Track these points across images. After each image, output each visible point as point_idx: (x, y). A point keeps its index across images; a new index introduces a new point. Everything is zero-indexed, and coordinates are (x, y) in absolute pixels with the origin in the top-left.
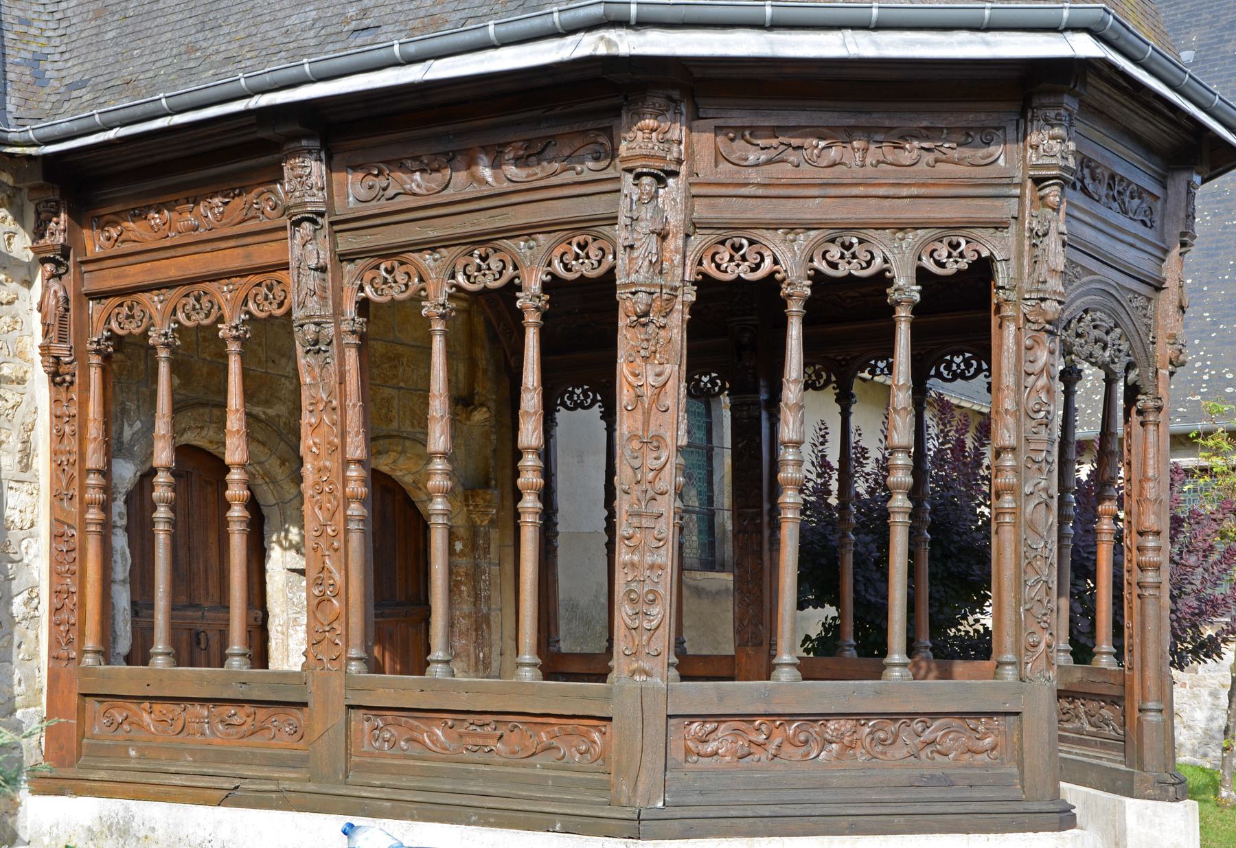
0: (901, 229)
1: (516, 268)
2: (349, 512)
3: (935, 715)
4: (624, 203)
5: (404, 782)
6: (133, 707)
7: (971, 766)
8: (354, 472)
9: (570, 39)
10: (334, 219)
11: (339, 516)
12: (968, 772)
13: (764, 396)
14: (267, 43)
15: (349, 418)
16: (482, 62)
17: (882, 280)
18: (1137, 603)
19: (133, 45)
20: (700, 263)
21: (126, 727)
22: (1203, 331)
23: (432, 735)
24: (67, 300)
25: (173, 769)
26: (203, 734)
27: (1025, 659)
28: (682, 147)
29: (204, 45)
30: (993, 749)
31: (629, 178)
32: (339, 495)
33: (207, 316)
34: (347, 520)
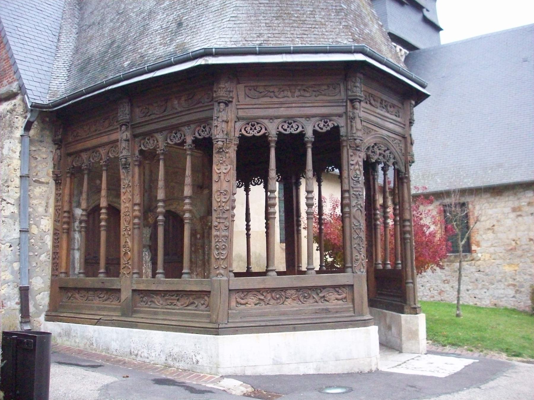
7: (337, 305)
13: (294, 181)
17: (302, 135)
21: (72, 298)
24: (61, 156)
27: (354, 265)
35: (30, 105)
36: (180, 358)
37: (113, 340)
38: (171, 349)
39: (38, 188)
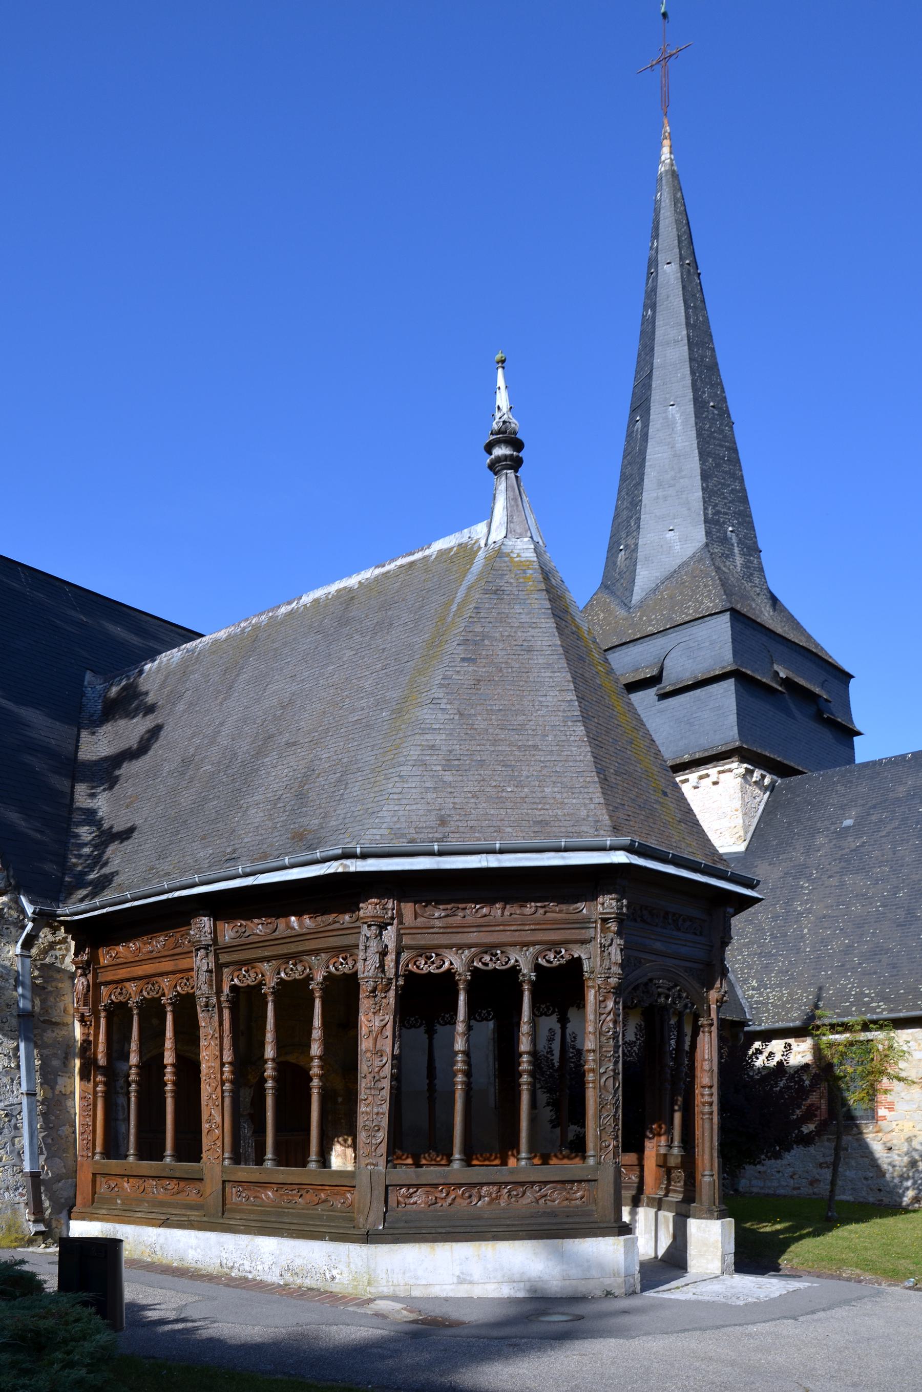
0: (525, 946)
1: (310, 970)
2: (224, 1088)
3: (546, 1183)
4: (362, 939)
5: (252, 1217)
6: (120, 1180)
8: (227, 1068)
9: (328, 864)
10: (216, 947)
11: (219, 1089)
12: (566, 1209)
14: (186, 866)
15: (225, 1042)
16: (282, 875)
18: (700, 1122)
19: (126, 866)
20: (407, 966)
21: (116, 1189)
22: (853, 968)
23: (266, 1195)
24: (88, 986)
25: (138, 1210)
26: (153, 1193)
28: (395, 911)
29: (158, 866)
30: (582, 1198)
31: (365, 926)
32: (219, 1079)
33: (157, 993)
34: (223, 1092)
35: (32, 911)
36: (305, 1272)
37: (192, 1248)
38: (289, 1262)
39: (49, 1031)
